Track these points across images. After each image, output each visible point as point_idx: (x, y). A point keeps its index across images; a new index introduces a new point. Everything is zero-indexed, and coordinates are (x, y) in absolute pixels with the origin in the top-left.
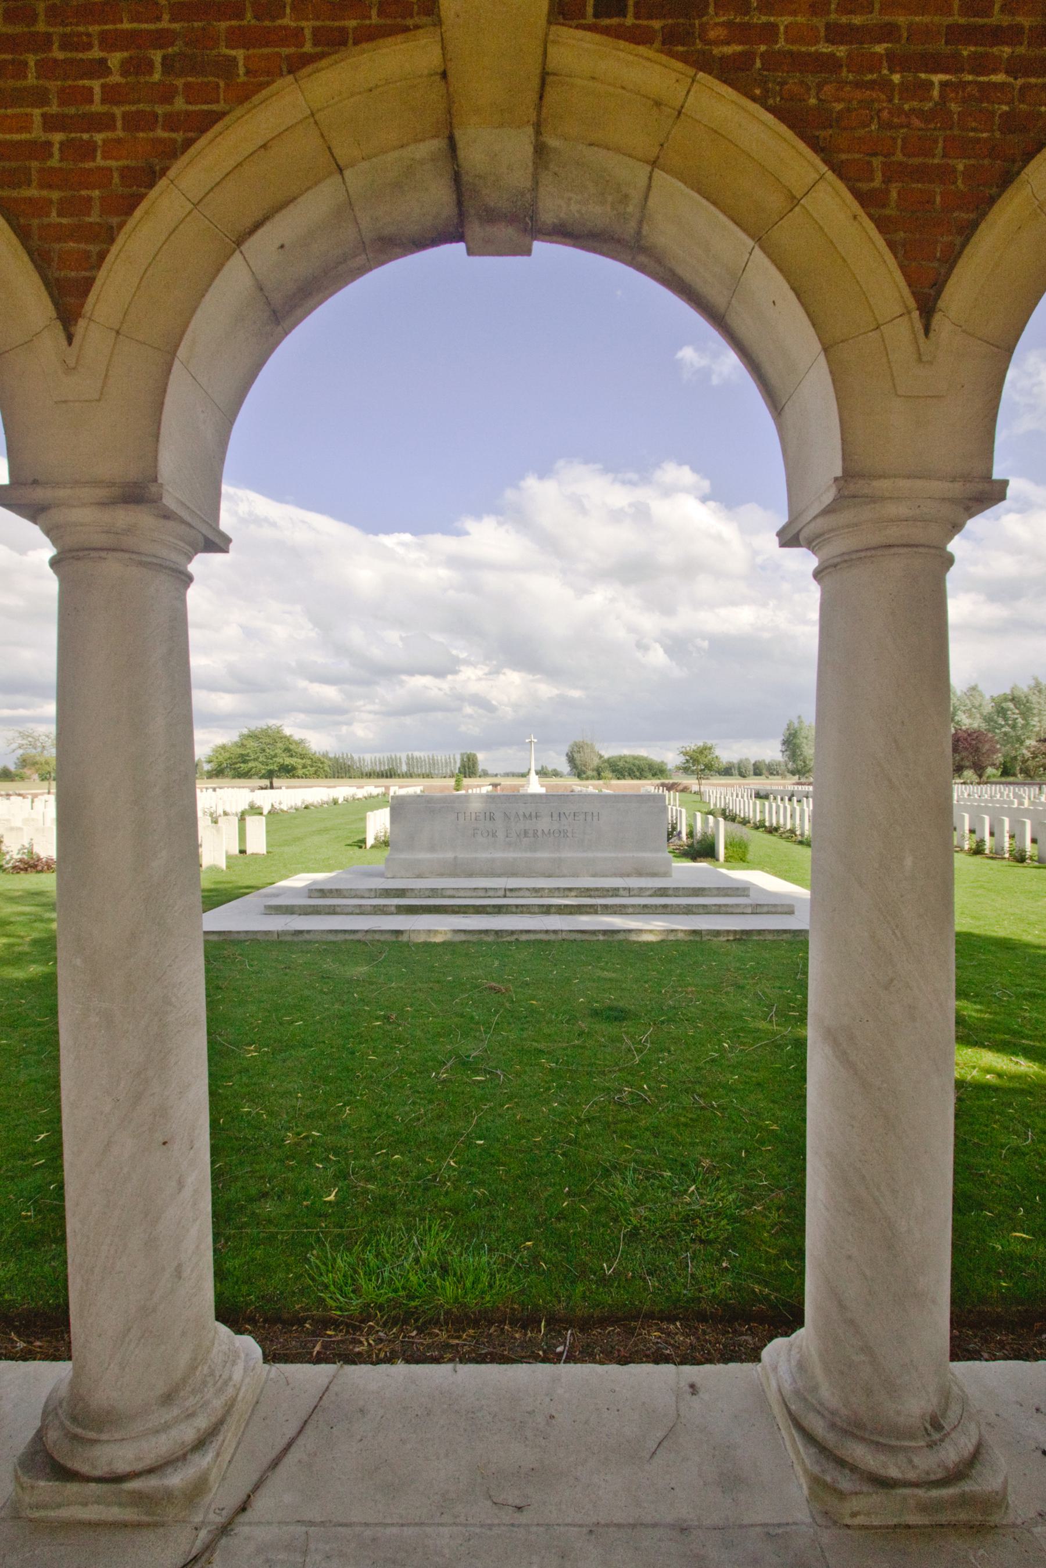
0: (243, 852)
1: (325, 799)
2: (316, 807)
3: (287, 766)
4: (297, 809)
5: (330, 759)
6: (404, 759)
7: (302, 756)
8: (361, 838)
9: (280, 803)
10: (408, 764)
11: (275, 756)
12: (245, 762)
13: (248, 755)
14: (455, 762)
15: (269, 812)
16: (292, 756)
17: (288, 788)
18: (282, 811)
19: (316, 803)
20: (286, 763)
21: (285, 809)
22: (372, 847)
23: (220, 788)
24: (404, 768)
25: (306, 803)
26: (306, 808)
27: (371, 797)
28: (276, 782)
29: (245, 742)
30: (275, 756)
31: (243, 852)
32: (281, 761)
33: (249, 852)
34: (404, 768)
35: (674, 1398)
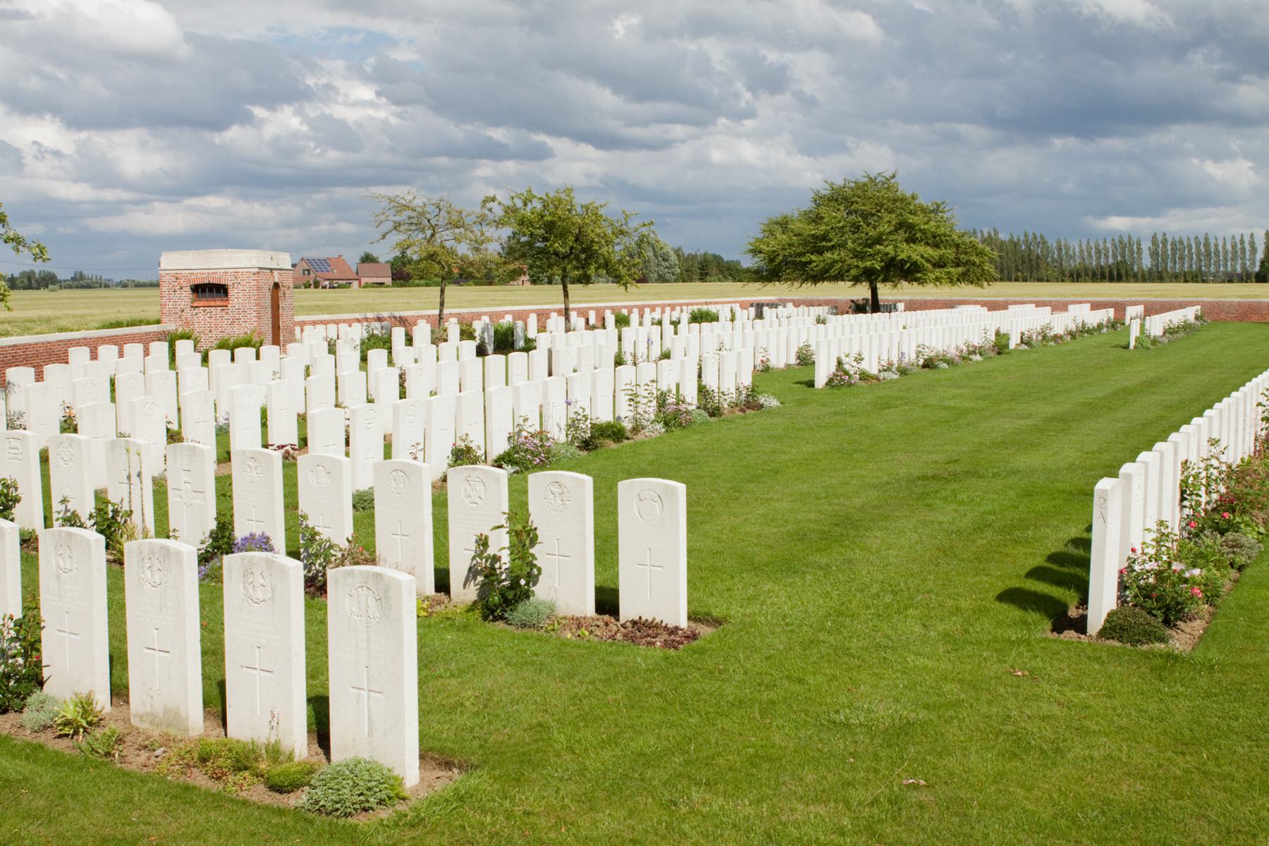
0: (607, 602)
1: (977, 341)
2: (950, 362)
3: (903, 262)
4: (903, 372)
5: (1001, 246)
6: (1146, 245)
7: (935, 241)
8: (1055, 539)
9: (859, 359)
10: (1154, 254)
11: (878, 240)
12: (820, 252)
13: (824, 238)
14: (1254, 250)
15: (830, 382)
16: (911, 240)
17: (912, 306)
18: (865, 376)
19: (953, 352)
20: (902, 256)
21: (874, 370)
22: (1113, 628)
23: (773, 305)
24: (1147, 262)
25: (928, 353)
26: (929, 365)
27: (1084, 331)
28: (886, 292)
29: (822, 211)
30: (878, 240)
31: (607, 602)
32: (890, 249)
33: (628, 611)
34: (1147, 262)
35: (1095, 448)
